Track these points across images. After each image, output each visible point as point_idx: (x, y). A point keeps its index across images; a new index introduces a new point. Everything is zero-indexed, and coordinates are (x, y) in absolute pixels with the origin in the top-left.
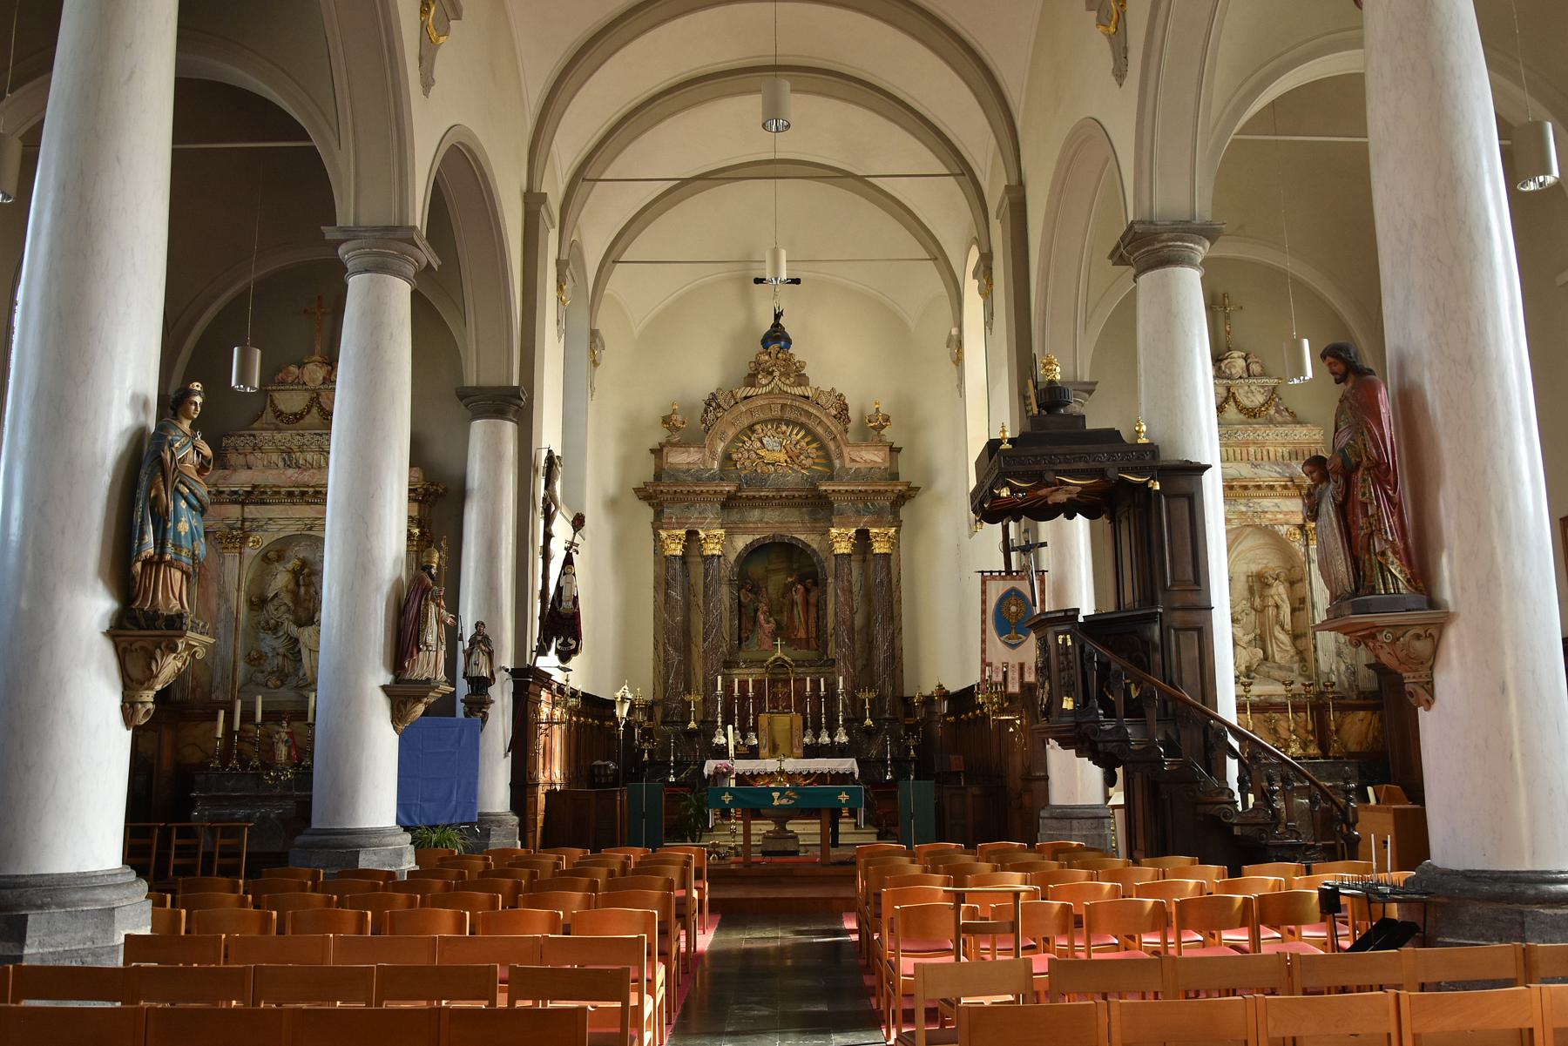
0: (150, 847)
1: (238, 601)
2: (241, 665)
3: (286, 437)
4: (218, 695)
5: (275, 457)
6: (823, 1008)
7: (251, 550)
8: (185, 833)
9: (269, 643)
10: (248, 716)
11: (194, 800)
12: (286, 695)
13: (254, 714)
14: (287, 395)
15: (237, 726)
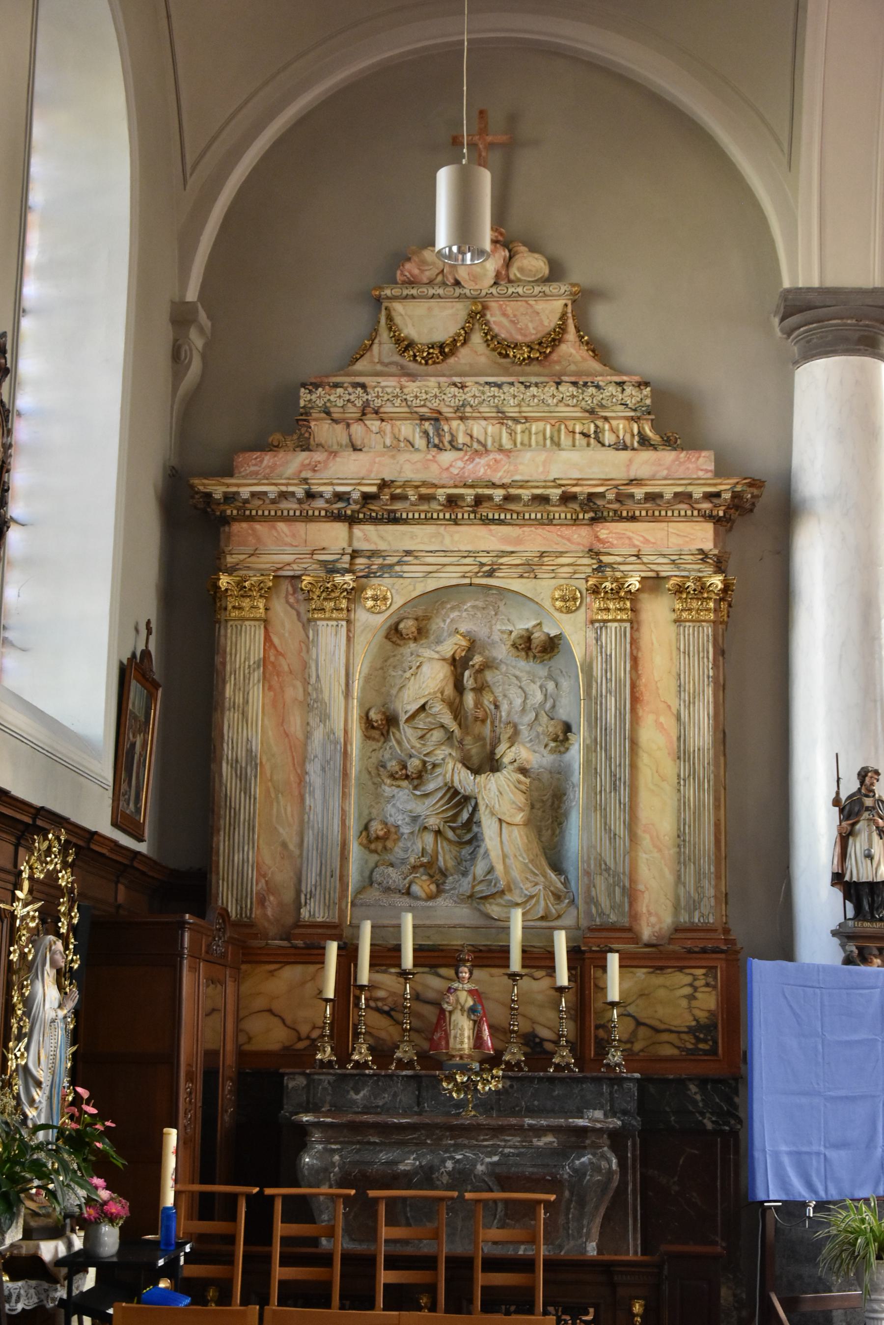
0: (231, 1239)
1: (344, 716)
2: (355, 849)
3: (427, 389)
4: (315, 911)
5: (407, 429)
6: (329, 1120)
7: (370, 621)
8: (300, 1209)
9: (402, 805)
10: (386, 955)
11: (303, 1131)
12: (452, 914)
13: (397, 949)
14: (418, 309)
15: (364, 976)
